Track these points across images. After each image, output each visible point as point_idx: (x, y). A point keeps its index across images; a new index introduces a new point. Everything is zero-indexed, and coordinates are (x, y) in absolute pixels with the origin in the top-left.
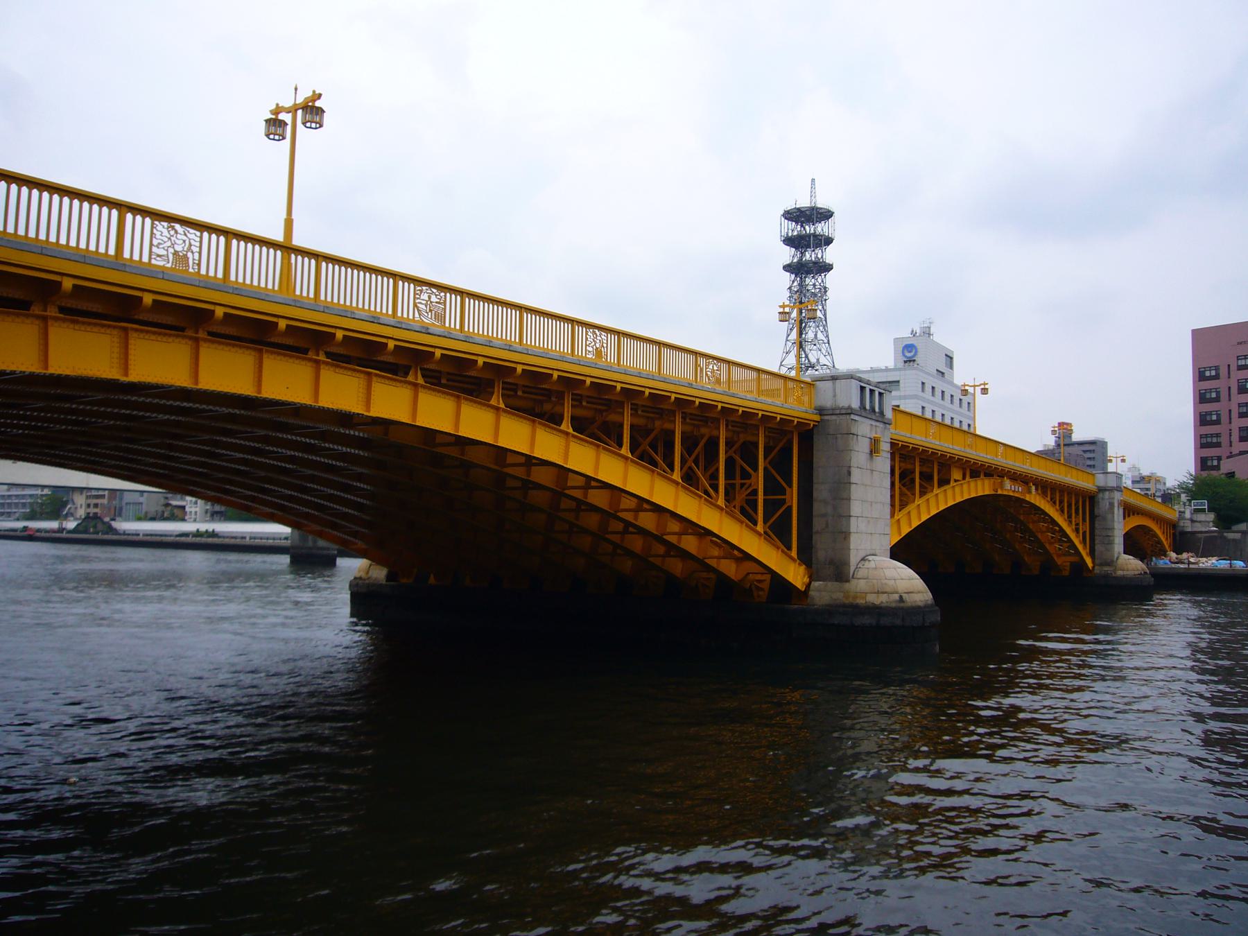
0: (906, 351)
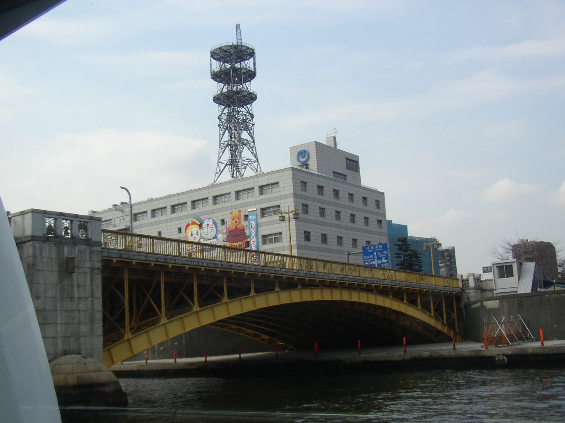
0: (300, 157)
